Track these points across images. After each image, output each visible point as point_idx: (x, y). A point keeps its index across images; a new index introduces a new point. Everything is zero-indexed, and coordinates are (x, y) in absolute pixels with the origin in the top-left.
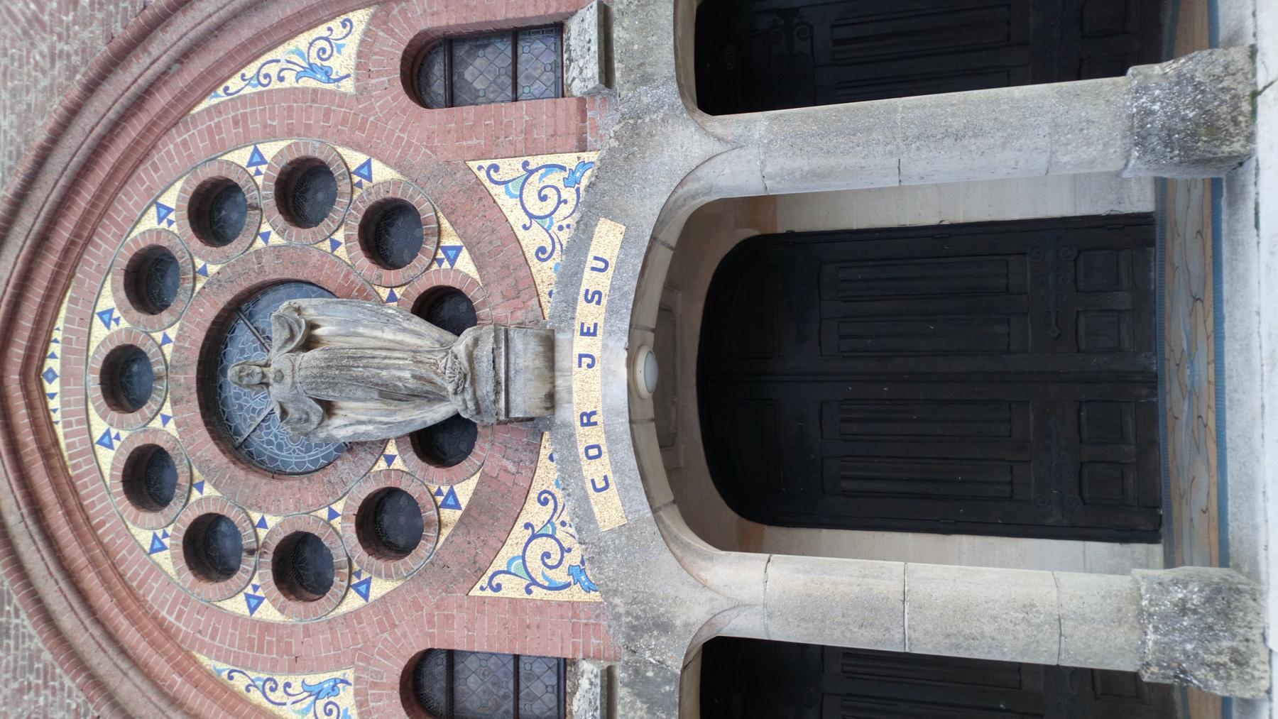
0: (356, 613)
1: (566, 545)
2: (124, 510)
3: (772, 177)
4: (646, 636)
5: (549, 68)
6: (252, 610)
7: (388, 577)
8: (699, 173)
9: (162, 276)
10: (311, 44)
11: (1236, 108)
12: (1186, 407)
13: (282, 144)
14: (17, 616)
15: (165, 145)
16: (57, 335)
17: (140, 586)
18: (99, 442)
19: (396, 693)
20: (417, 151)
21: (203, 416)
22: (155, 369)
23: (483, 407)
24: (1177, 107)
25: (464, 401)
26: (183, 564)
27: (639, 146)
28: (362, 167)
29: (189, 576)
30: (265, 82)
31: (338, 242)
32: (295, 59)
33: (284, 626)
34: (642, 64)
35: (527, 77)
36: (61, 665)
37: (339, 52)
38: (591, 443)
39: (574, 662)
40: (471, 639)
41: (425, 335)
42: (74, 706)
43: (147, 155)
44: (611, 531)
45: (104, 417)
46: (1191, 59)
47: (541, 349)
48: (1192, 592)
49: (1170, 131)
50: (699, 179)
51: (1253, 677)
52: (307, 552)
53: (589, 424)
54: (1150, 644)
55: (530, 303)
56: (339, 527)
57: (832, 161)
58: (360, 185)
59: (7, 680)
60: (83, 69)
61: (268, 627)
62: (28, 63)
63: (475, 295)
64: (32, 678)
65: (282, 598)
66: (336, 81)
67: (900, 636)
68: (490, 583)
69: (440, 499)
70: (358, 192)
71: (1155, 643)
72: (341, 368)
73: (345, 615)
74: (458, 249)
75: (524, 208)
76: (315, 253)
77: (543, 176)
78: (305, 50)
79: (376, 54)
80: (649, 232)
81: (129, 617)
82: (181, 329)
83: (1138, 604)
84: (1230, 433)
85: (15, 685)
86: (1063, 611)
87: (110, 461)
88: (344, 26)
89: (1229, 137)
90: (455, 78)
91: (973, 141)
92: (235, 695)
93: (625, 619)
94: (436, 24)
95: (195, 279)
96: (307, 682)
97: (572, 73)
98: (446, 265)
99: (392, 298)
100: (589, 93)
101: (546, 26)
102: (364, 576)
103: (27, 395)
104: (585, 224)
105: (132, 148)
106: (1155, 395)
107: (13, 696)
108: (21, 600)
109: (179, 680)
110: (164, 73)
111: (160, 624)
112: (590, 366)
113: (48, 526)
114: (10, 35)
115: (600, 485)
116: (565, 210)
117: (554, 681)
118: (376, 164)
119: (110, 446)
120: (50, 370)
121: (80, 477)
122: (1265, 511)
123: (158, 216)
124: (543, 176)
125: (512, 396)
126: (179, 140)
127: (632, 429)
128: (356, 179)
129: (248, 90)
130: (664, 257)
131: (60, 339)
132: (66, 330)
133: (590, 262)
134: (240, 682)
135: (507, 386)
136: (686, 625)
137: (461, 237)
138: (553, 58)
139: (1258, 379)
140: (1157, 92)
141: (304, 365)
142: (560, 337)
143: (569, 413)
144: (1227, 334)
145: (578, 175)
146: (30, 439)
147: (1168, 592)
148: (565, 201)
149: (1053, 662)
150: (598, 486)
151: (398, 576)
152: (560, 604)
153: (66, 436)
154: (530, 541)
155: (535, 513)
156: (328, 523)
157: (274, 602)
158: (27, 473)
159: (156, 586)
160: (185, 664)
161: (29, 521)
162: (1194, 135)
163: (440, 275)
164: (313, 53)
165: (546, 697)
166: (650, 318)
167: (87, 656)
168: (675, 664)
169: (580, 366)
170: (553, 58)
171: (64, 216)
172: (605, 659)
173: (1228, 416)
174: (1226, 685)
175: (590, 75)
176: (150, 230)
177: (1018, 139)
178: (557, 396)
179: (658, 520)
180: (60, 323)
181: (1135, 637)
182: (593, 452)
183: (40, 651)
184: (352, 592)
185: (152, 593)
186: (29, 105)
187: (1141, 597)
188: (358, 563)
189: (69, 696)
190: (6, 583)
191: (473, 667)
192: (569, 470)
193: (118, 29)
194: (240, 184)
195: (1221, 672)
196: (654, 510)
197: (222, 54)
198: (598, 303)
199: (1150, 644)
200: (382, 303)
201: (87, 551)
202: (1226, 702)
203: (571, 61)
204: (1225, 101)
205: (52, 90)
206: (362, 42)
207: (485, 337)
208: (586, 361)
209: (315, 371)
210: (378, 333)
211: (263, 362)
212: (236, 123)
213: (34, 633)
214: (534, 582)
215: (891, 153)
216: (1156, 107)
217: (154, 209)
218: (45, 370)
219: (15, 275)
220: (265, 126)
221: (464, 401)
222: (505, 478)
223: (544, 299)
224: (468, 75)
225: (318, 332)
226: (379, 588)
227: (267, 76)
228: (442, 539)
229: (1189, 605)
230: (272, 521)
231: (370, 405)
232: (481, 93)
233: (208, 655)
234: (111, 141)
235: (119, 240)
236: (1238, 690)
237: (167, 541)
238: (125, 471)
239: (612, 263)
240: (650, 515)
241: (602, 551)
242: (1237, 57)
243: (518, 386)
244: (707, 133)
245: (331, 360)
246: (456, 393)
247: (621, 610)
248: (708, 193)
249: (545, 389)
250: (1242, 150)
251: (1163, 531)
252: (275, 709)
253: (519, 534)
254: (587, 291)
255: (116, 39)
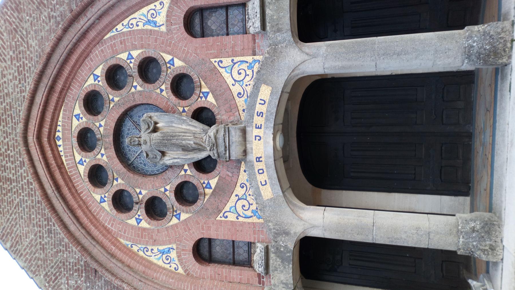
0: (176, 225)
1: (251, 203)
2: (90, 187)
3: (327, 68)
4: (281, 237)
5: (240, 21)
6: (138, 224)
7: (187, 212)
8: (299, 67)
9: (97, 101)
10: (148, 12)
11: (505, 45)
12: (481, 149)
13: (139, 51)
14: (54, 226)
15: (95, 51)
16: (59, 123)
17: (97, 215)
18: (79, 163)
19: (191, 253)
20: (191, 55)
21: (116, 154)
22: (97, 137)
23: (220, 155)
24: (483, 44)
25: (214, 153)
26: (112, 207)
27: (276, 56)
28: (170, 60)
29: (114, 211)
30: (131, 27)
31: (162, 90)
32: (142, 17)
33: (150, 229)
34: (277, 24)
35: (232, 24)
36: (72, 243)
37: (159, 15)
38: (260, 168)
39: (254, 243)
40: (217, 235)
41: (197, 127)
42: (77, 257)
43: (88, 55)
44: (268, 200)
45: (79, 154)
46: (489, 25)
47: (241, 134)
48: (477, 224)
49: (480, 54)
50: (299, 69)
51: (497, 254)
52: (156, 202)
53: (259, 161)
54: (461, 242)
55: (236, 114)
56: (168, 195)
57: (350, 63)
58: (170, 68)
59: (52, 248)
60: (62, 23)
61: (144, 229)
62: (40, 20)
63: (215, 111)
64: (61, 248)
65: (149, 220)
66: (158, 26)
67: (372, 238)
68: (223, 215)
69: (204, 185)
70: (169, 71)
71: (463, 242)
72: (168, 140)
73: (172, 226)
74: (208, 93)
75: (232, 77)
76: (154, 94)
77: (239, 65)
78: (146, 14)
79: (174, 16)
80: (281, 90)
81: (94, 226)
82: (106, 122)
83: (457, 228)
84: (496, 165)
85: (55, 250)
86: (430, 230)
87: (83, 170)
88: (161, 4)
89: (502, 57)
90: (204, 24)
91: (404, 56)
92: (134, 253)
93: (273, 231)
94: (196, 4)
95: (110, 103)
96: (159, 248)
97: (249, 24)
98: (204, 99)
99: (184, 111)
100: (256, 33)
101: (239, 4)
102: (178, 212)
103: (51, 146)
104: (257, 87)
105: (82, 53)
106: (471, 141)
107: (55, 254)
108: (55, 220)
109: (114, 248)
110: (93, 24)
111: (105, 228)
112: (259, 140)
113: (63, 194)
114: (32, 8)
115: (264, 183)
116: (248, 78)
117: (247, 249)
118: (176, 60)
119: (83, 165)
120: (58, 136)
121: (72, 175)
122: (505, 197)
123: (94, 79)
124: (239, 65)
125: (231, 151)
126: (100, 49)
127: (275, 163)
128: (168, 65)
129: (125, 30)
130: (286, 96)
131: (61, 125)
132: (63, 122)
133: (259, 101)
134: (135, 248)
135: (229, 148)
136: (295, 233)
137: (209, 88)
138: (242, 17)
139: (506, 148)
140: (475, 38)
141: (154, 138)
142: (248, 129)
143: (252, 157)
144: (497, 128)
145: (253, 65)
146: (53, 162)
147: (469, 224)
148: (248, 75)
149: (426, 247)
150: (263, 184)
151: (190, 212)
152: (249, 223)
153: (66, 161)
154: (237, 201)
155: (239, 191)
156: (164, 193)
157: (146, 221)
158: (53, 175)
159: (103, 215)
160: (115, 242)
161: (56, 192)
162: (489, 56)
163: (201, 103)
164: (149, 16)
165: (244, 254)
166: (280, 120)
167: (80, 240)
168: (291, 245)
169: (255, 140)
170: (242, 17)
171: (59, 79)
172: (266, 243)
173: (496, 158)
174: (487, 257)
175: (257, 26)
176: (91, 84)
177: (422, 56)
178: (247, 151)
179: (285, 196)
180: (60, 119)
181: (455, 240)
182: (261, 171)
183: (63, 238)
184: (174, 218)
185: (102, 217)
186: (42, 37)
187: (459, 225)
188: (176, 207)
189: (75, 254)
190: (49, 215)
191: (218, 243)
192: (252, 178)
193: (74, 7)
194: (125, 67)
195: (486, 252)
196: (283, 192)
197: (114, 16)
198: (262, 116)
199: (461, 242)
200: (180, 114)
201: (77, 202)
202: (488, 263)
203: (249, 19)
204: (501, 43)
205: (50, 31)
206: (168, 11)
207: (220, 130)
208: (258, 138)
209: (159, 141)
210: (180, 126)
211: (138, 136)
212: (121, 43)
213: (61, 232)
214: (239, 215)
215: (373, 60)
216: (475, 44)
217: (92, 76)
218: (56, 136)
219: (42, 102)
220: (132, 44)
221: (214, 153)
222: (227, 178)
223: (241, 112)
224: (209, 23)
225: (158, 125)
226: (184, 216)
227: (132, 24)
228: (206, 200)
229: (475, 229)
230: (144, 192)
231: (178, 152)
232: (214, 31)
233: (123, 239)
234: (74, 50)
235: (80, 88)
236: (491, 259)
237: (106, 199)
238: (89, 173)
239: (267, 101)
240: (281, 194)
241: (266, 207)
242: (507, 25)
243: (233, 148)
244: (303, 52)
245: (164, 137)
246: (210, 150)
247: (272, 227)
248: (303, 74)
249: (243, 148)
250: (507, 62)
251: (471, 192)
252: (148, 258)
253: (233, 198)
254: (258, 112)
255: (74, 11)
